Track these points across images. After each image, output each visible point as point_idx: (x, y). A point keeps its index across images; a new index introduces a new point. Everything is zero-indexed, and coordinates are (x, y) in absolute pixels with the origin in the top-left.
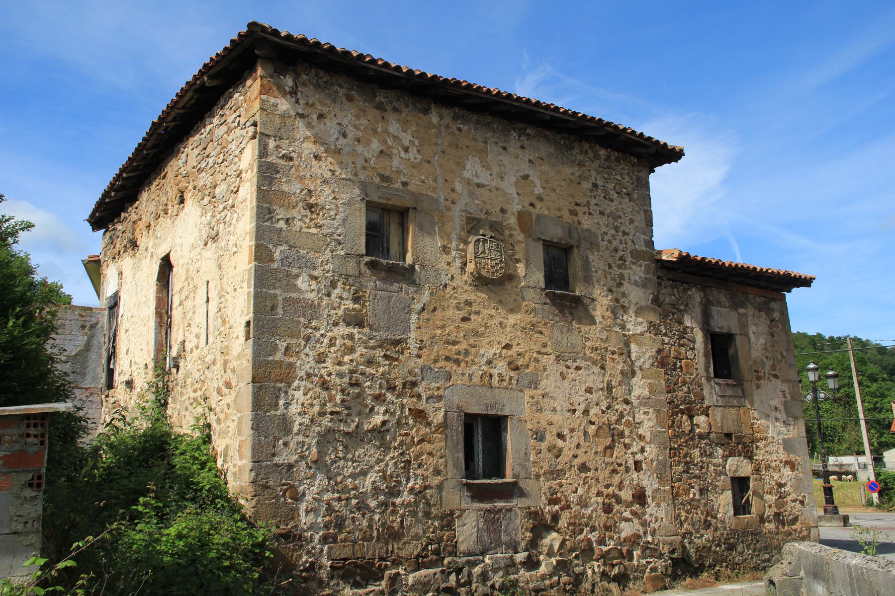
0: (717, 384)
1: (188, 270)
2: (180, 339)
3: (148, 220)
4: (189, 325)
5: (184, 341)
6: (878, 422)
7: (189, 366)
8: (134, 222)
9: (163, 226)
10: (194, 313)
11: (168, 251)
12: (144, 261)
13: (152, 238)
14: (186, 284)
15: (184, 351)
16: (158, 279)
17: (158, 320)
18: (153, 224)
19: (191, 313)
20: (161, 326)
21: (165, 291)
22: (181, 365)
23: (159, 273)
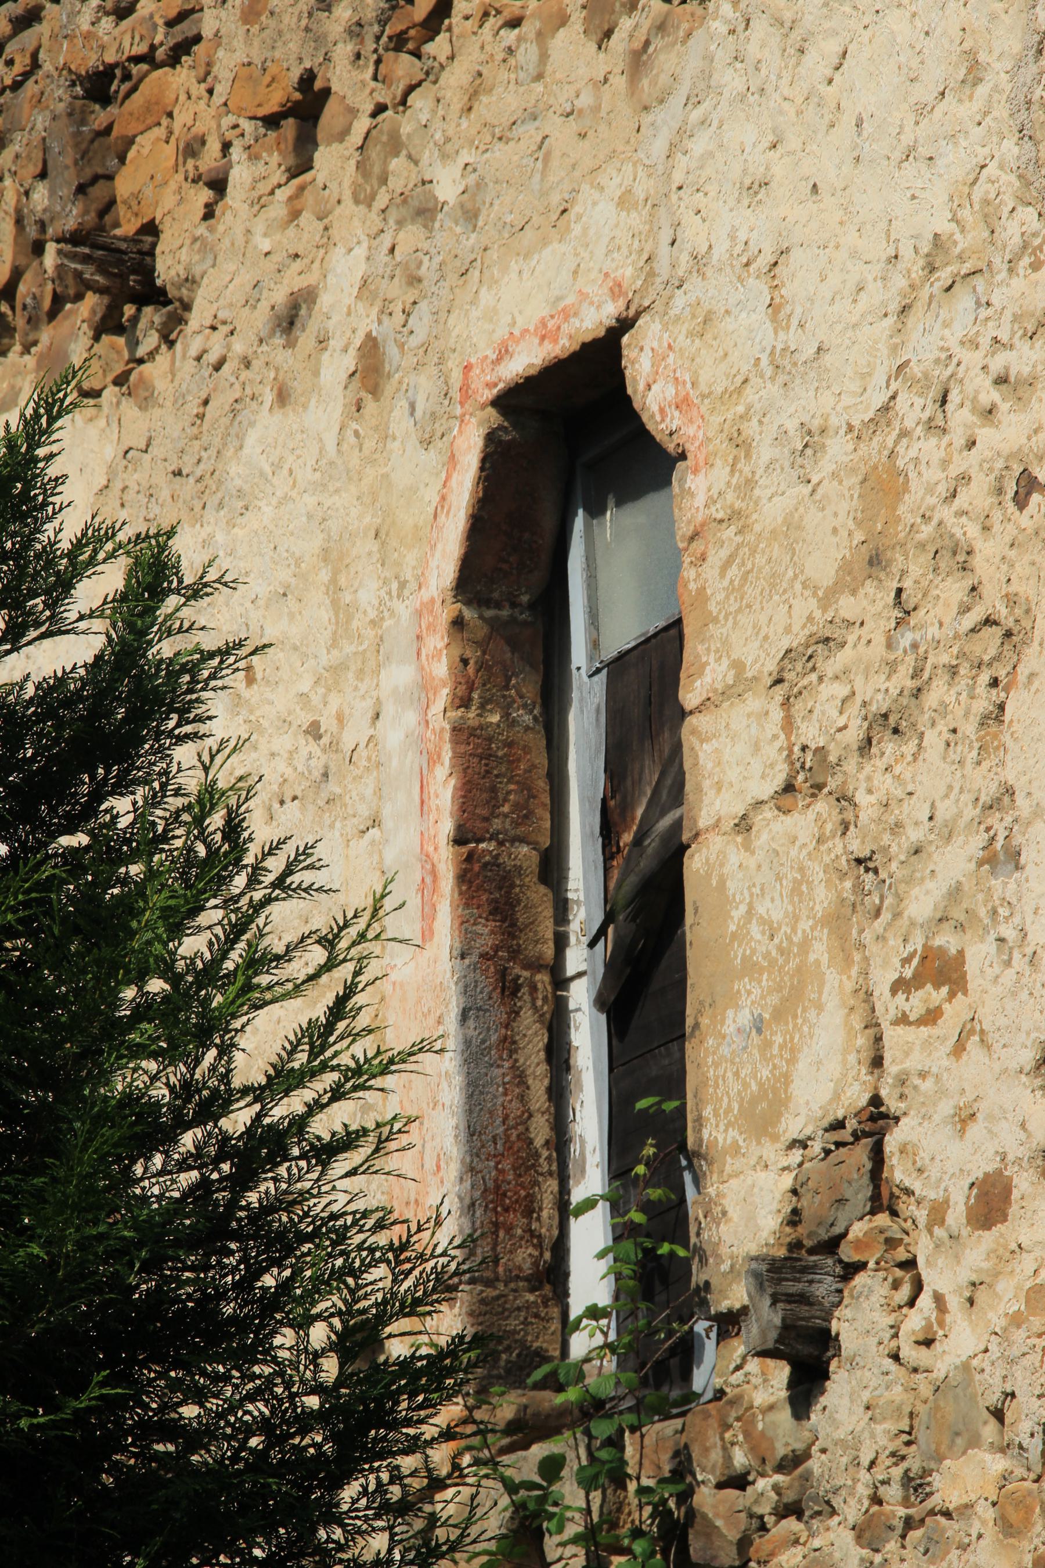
0: (353, 1173)
1: (884, 485)
2: (824, 1084)
3: (291, 58)
4: (942, 970)
5: (877, 1119)
6: (515, 1376)
7: (962, 1341)
8: (99, 86)
9: (504, 101)
10: (1002, 857)
11: (592, 321)
12: (265, 425)
13: (353, 222)
14: (871, 603)
15: (882, 1199)
16: (471, 582)
17: (486, 935)
18: (349, 83)
19: (955, 861)
20: (509, 988)
21: (527, 685)
22: (861, 1319)
23: (479, 527)
